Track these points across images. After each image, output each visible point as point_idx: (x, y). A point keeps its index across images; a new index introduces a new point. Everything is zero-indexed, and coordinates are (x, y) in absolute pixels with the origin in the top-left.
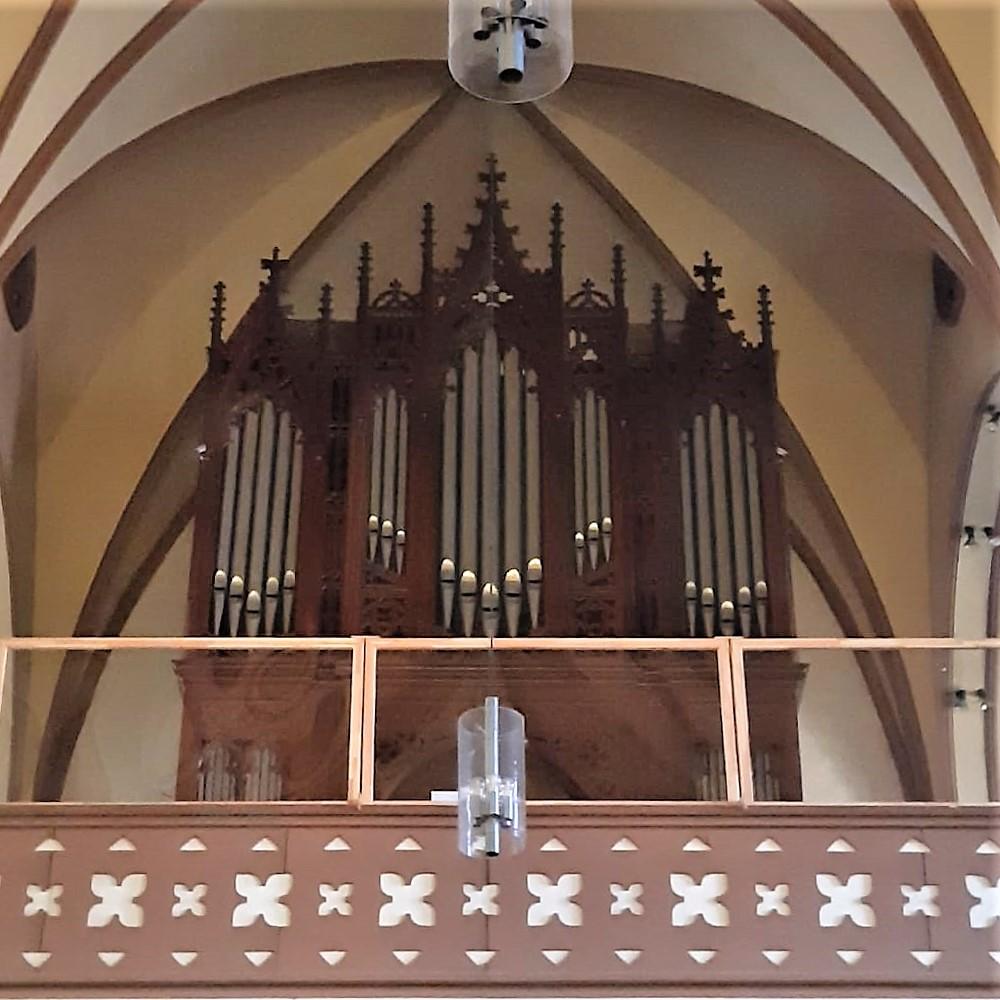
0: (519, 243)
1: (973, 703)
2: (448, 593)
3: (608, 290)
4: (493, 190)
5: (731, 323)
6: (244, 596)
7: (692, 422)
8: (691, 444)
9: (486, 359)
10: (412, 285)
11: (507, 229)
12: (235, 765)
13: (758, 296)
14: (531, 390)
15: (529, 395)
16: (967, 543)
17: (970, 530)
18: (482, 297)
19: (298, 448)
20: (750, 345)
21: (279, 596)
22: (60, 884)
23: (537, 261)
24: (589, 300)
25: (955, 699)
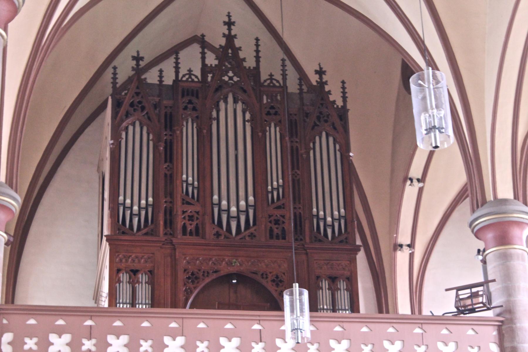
0: (242, 55)
1: (406, 249)
2: (216, 210)
3: (279, 78)
4: (230, 29)
5: (330, 96)
6: (131, 208)
7: (315, 138)
8: (314, 149)
9: (229, 106)
10: (197, 72)
11: (237, 48)
12: (131, 280)
13: (341, 85)
14: (248, 121)
15: (247, 123)
16: (410, 185)
17: (411, 180)
18: (226, 78)
19: (151, 143)
20: (338, 106)
21: (146, 209)
22: (96, 338)
23: (250, 63)
24: (271, 82)
25: (399, 248)
